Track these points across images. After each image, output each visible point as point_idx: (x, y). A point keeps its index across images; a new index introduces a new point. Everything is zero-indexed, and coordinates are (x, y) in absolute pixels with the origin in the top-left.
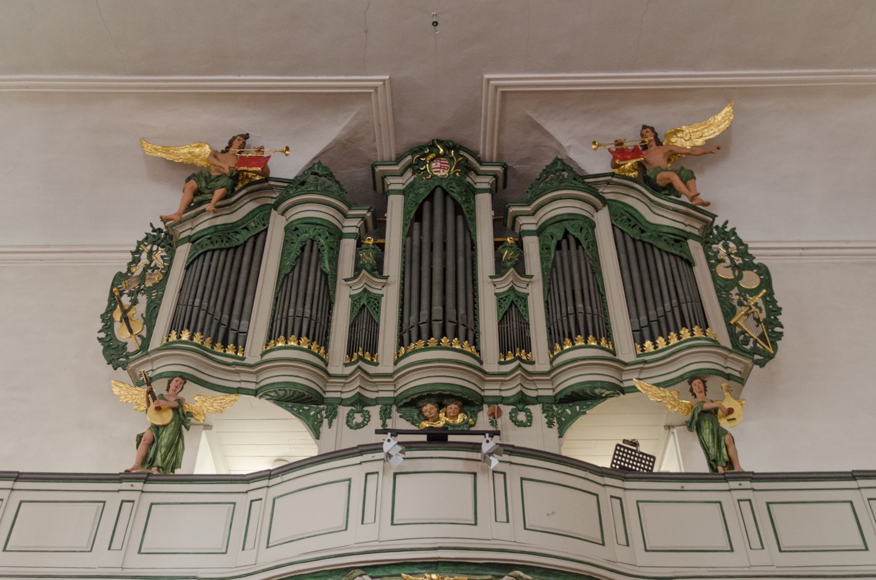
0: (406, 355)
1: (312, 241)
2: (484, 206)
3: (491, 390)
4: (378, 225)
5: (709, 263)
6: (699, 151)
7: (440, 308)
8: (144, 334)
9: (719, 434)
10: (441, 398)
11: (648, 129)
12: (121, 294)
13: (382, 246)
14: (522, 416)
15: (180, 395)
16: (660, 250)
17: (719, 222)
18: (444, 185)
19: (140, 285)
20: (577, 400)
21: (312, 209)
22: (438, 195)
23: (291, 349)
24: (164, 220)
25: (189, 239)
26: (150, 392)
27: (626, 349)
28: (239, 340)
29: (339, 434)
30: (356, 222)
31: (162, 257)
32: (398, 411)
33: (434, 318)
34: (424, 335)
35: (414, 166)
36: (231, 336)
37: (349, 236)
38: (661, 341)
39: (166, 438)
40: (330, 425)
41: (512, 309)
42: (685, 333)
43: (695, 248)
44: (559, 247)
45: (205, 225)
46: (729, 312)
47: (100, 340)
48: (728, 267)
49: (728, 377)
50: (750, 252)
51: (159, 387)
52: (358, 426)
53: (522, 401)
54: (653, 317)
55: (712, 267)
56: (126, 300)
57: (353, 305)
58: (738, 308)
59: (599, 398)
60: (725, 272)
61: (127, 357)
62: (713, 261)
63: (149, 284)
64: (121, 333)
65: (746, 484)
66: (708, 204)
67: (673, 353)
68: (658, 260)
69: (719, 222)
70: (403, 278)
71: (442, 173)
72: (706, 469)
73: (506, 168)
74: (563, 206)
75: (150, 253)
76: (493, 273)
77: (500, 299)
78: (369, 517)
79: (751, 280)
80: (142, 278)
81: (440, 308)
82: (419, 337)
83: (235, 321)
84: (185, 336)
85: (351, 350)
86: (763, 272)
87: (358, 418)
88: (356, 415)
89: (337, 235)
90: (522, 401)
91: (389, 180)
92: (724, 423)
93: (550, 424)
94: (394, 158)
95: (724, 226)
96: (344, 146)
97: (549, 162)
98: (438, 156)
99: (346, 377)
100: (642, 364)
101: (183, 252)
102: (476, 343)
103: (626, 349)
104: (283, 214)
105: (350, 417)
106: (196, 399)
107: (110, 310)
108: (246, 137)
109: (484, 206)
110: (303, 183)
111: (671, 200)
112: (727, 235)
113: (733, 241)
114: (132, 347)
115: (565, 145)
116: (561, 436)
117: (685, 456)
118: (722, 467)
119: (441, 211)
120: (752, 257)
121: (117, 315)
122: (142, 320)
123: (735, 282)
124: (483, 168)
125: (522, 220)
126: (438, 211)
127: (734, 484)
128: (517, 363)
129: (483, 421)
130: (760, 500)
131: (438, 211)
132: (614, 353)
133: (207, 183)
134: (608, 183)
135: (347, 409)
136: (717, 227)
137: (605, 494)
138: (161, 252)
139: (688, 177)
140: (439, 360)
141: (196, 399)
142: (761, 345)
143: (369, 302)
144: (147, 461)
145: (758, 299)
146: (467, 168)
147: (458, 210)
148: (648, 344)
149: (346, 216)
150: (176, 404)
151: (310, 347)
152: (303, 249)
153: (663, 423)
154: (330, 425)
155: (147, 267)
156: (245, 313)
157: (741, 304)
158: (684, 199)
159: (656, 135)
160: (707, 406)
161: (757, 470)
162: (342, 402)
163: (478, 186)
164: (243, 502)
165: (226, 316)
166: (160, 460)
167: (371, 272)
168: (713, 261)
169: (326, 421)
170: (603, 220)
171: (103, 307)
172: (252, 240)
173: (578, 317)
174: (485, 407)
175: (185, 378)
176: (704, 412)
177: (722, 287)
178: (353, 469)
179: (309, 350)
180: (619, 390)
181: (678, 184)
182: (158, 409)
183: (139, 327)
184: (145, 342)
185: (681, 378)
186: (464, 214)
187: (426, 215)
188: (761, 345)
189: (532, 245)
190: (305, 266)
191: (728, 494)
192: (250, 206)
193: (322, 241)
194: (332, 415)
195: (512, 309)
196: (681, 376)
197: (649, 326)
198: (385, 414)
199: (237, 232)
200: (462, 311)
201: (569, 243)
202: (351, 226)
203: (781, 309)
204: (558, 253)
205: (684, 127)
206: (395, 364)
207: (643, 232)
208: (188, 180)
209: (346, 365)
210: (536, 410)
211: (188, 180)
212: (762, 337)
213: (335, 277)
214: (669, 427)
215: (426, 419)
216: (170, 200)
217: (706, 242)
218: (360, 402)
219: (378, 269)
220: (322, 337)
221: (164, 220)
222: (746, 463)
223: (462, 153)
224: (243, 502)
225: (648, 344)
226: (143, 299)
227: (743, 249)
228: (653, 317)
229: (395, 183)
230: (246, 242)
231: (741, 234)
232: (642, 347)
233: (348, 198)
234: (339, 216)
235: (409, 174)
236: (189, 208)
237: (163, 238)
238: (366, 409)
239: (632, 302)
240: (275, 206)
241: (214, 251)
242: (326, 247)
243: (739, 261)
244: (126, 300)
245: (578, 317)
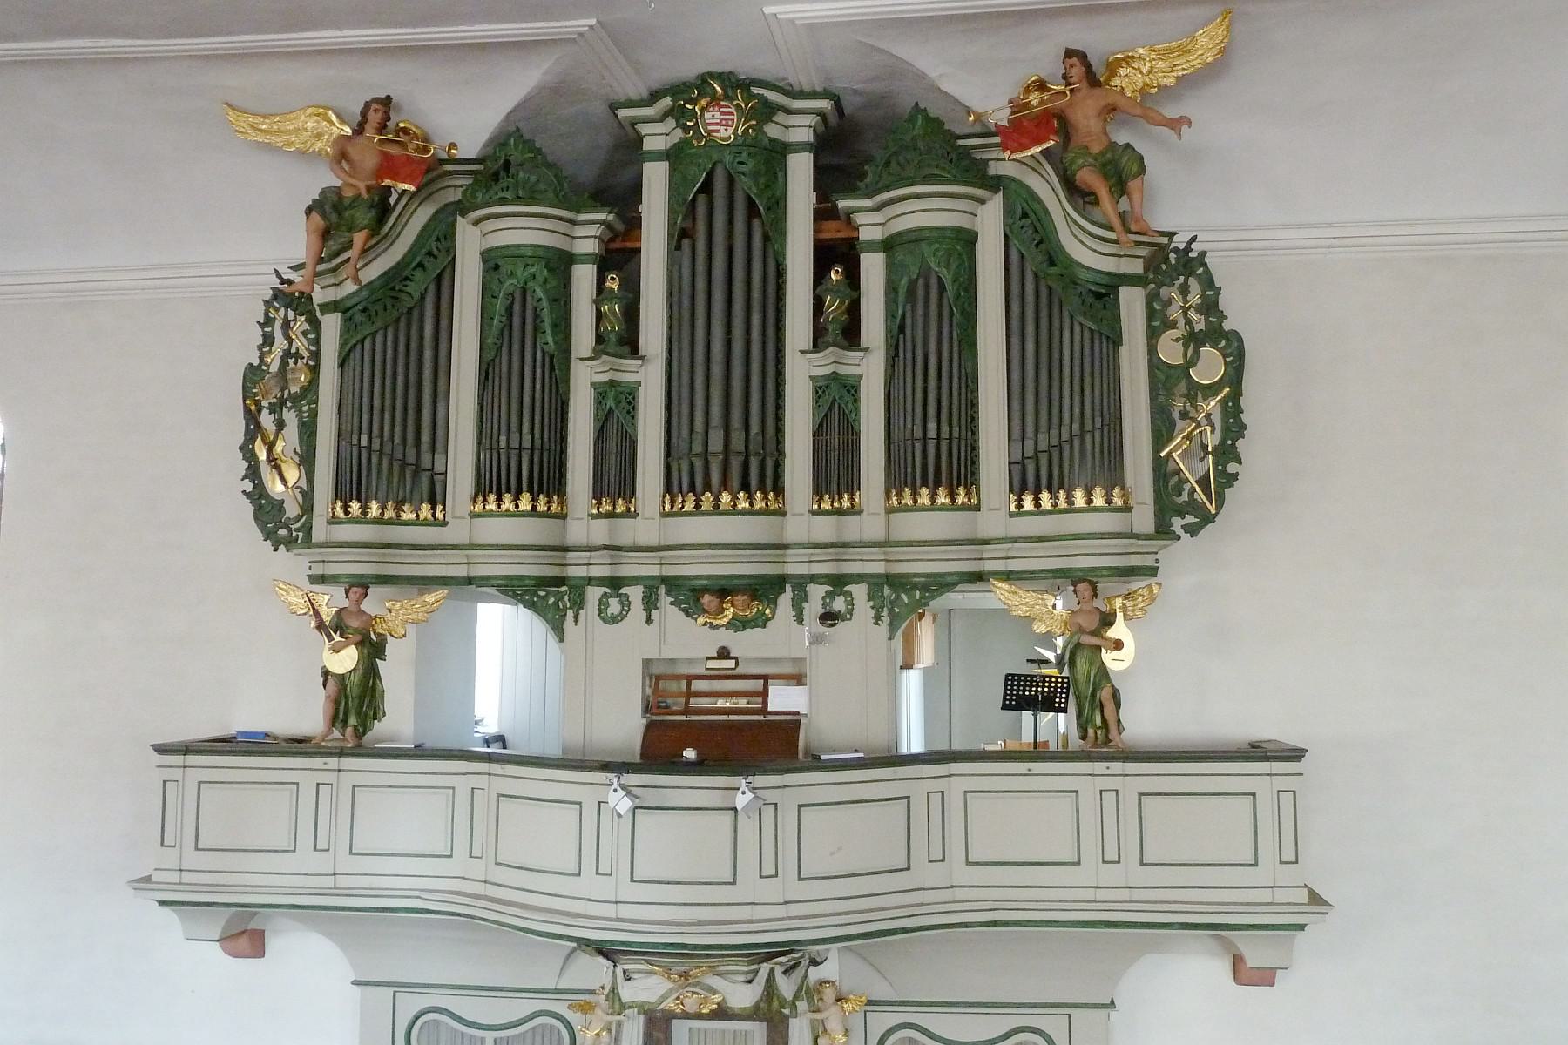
1: (524, 291)
4: (619, 257)
5: (1149, 326)
8: (303, 484)
11: (1075, 60)
12: (259, 410)
19: (282, 391)
21: (522, 228)
31: (304, 333)
32: (668, 593)
33: (711, 449)
35: (677, 113)
41: (836, 400)
43: (1131, 302)
46: (1162, 432)
48: (1177, 340)
52: (615, 620)
54: (1043, 446)
55: (1153, 335)
58: (1180, 424)
60: (1171, 351)
61: (287, 527)
62: (1157, 323)
63: (294, 389)
64: (276, 488)
68: (1072, 316)
70: (670, 351)
71: (724, 134)
74: (926, 209)
75: (286, 325)
76: (808, 345)
87: (614, 607)
88: (612, 601)
93: (877, 619)
94: (645, 94)
95: (1188, 249)
96: (555, 91)
98: (715, 100)
101: (332, 325)
105: (603, 604)
107: (250, 437)
108: (387, 102)
113: (1198, 277)
115: (933, 73)
119: (728, 204)
122: (297, 459)
133: (340, 214)
136: (1176, 250)
137: (918, 791)
143: (618, 403)
146: (767, 111)
151: (534, 508)
155: (287, 354)
156: (438, 443)
157: (1184, 415)
159: (1088, 67)
168: (1156, 324)
169: (570, 613)
171: (240, 439)
172: (432, 288)
174: (788, 587)
177: (1163, 379)
183: (293, 474)
186: (766, 212)
189: (873, 267)
190: (516, 347)
192: (422, 215)
193: (540, 293)
194: (579, 603)
196: (1062, 570)
197: (1036, 458)
198: (650, 603)
199: (407, 279)
203: (1245, 427)
204: (909, 307)
205: (1141, 51)
207: (1052, 263)
210: (859, 591)
215: (705, 611)
216: (292, 243)
223: (755, 90)
226: (290, 416)
228: (1043, 446)
230: (423, 297)
232: (1020, 500)
233: (573, 195)
238: (623, 591)
239: (1016, 405)
242: (545, 303)
244: (267, 420)
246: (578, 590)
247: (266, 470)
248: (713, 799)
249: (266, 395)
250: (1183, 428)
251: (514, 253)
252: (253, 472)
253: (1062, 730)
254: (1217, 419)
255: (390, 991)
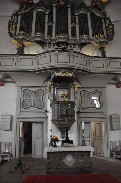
0: (57, 36)
2: (69, 10)
3: (70, 42)
4: (51, 13)
6: (106, 3)
7: (62, 29)
8: (15, 31)
9: (104, 51)
10: (62, 43)
13: (52, 17)
14: (75, 47)
15: (23, 42)
16: (98, 21)
17: (107, 16)
18: (63, 6)
20: (82, 45)
22: (62, 8)
23: (39, 35)
24: (16, 11)
25: (20, 15)
26: (18, 41)
27: (91, 37)
28: (30, 33)
29: (47, 49)
30: (48, 12)
34: (60, 32)
36: (29, 32)
37: (47, 15)
38: (97, 36)
39: (21, 48)
40: (45, 47)
41: (74, 29)
42: (100, 35)
43: (103, 20)
44: (82, 19)
45: (23, 12)
46: (107, 32)
47: (8, 32)
49: (106, 42)
50: (111, 22)
51: (19, 40)
52: (50, 47)
53: (75, 44)
55: (105, 24)
56: (11, 25)
57: (48, 27)
59: (87, 44)
60: (107, 25)
63: (15, 23)
64: (12, 32)
65: (107, 59)
66: (106, 13)
67: (98, 38)
68: (97, 23)
69: (107, 16)
72: (101, 56)
73: (73, 3)
75: (14, 17)
77: (72, 27)
78: (54, 61)
79: (111, 27)
80: (13, 22)
81: (62, 29)
82: (59, 33)
83: (29, 29)
84: (22, 32)
85: (48, 35)
86: (113, 25)
89: (45, 15)
90: (75, 44)
91: (53, 4)
92: (104, 49)
93: (79, 48)
97: (81, 3)
99: (47, 39)
100: (93, 40)
101: (20, 17)
102: (68, 34)
103: (91, 37)
104: (35, 10)
105: (48, 46)
106: (26, 43)
107: (9, 27)
109: (69, 10)
110: (39, 5)
111: (100, 12)
112: (108, 19)
114: (13, 34)
116: (80, 50)
117: (98, 53)
118: (104, 56)
120: (111, 23)
121: (10, 28)
123: (108, 27)
124: (69, 3)
125: (76, 13)
126: (62, 11)
127: (105, 58)
128: (74, 38)
129: (69, 46)
130: (108, 61)
131: (62, 11)
132: (89, 37)
134: (90, 7)
135: (48, 44)
138: (16, 17)
139: (104, 8)
140: (64, 37)
141: (26, 43)
142: (111, 38)
144: (19, 52)
145: (111, 30)
147: (65, 11)
148: (95, 36)
149: (46, 11)
150: (22, 43)
152: (39, 17)
153: (95, 48)
154: (45, 47)
155: (14, 20)
156: (31, 28)
158: (102, 12)
160: (103, 47)
161: (108, 57)
162: (47, 43)
163: (68, 6)
164: (34, 59)
165: (28, 29)
166: (20, 52)
167: (51, 21)
170: (89, 14)
173: (84, 31)
175: (23, 39)
176: (102, 47)
177: (106, 28)
178: (51, 54)
179: (42, 35)
180: (89, 43)
181: (102, 9)
182: (20, 44)
184: (16, 33)
185: (99, 42)
187: (60, 11)
188: (111, 38)
189: (77, 18)
191: (104, 60)
192: (30, 9)
194: (46, 45)
195: (74, 29)
197: (97, 32)
198: (54, 46)
200: (66, 29)
201: (83, 18)
202: (47, 13)
206: (55, 37)
208: (19, 3)
209: (47, 37)
210: (77, 46)
211: (19, 3)
212: (111, 36)
213: (45, 22)
214: (96, 49)
217: (105, 19)
218: (50, 43)
219: (52, 21)
220: (43, 32)
221: (16, 11)
222: (107, 56)
224: (34, 59)
225: (95, 36)
226: (14, 25)
227: (110, 21)
229: (54, 5)
231: (111, 19)
234: (45, 11)
235: (57, 3)
236: (20, 9)
237: (16, 14)
240: (34, 9)
241: (25, 17)
243: (109, 23)
244: (11, 25)
245: (84, 31)
246: (46, 44)
247: (11, 30)
248: (67, 54)
249: (12, 24)
250: (109, 32)
251: (40, 12)
252: (9, 30)
253: (55, 95)
254: (112, 31)
255: (21, 87)
